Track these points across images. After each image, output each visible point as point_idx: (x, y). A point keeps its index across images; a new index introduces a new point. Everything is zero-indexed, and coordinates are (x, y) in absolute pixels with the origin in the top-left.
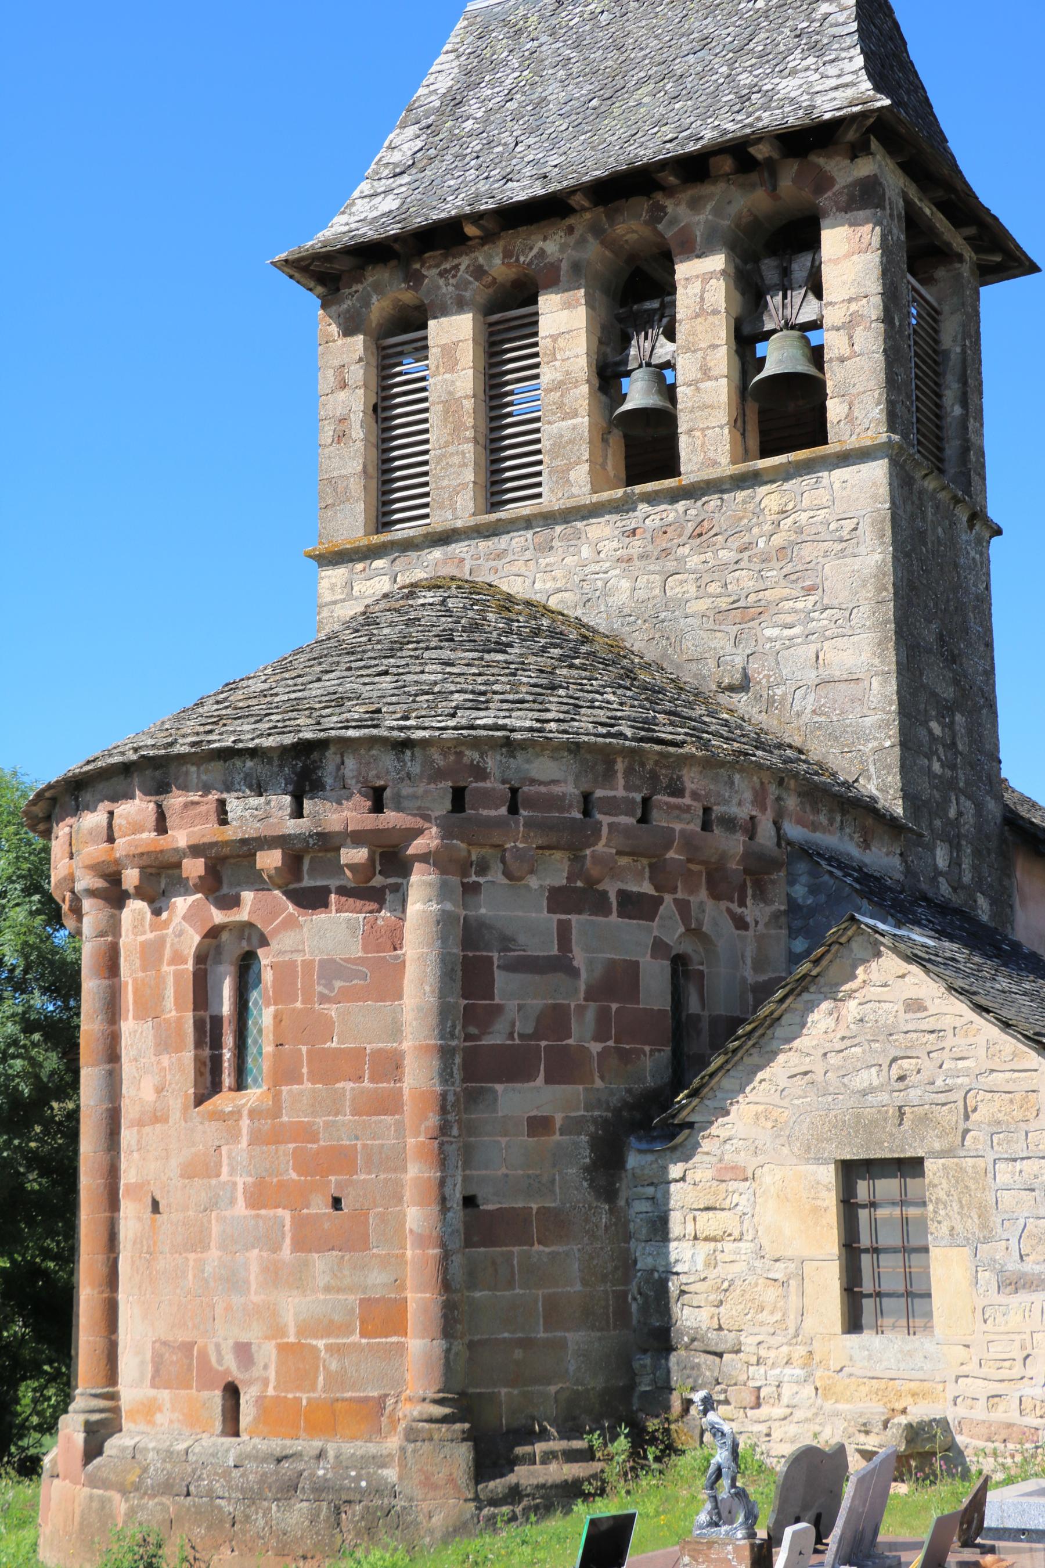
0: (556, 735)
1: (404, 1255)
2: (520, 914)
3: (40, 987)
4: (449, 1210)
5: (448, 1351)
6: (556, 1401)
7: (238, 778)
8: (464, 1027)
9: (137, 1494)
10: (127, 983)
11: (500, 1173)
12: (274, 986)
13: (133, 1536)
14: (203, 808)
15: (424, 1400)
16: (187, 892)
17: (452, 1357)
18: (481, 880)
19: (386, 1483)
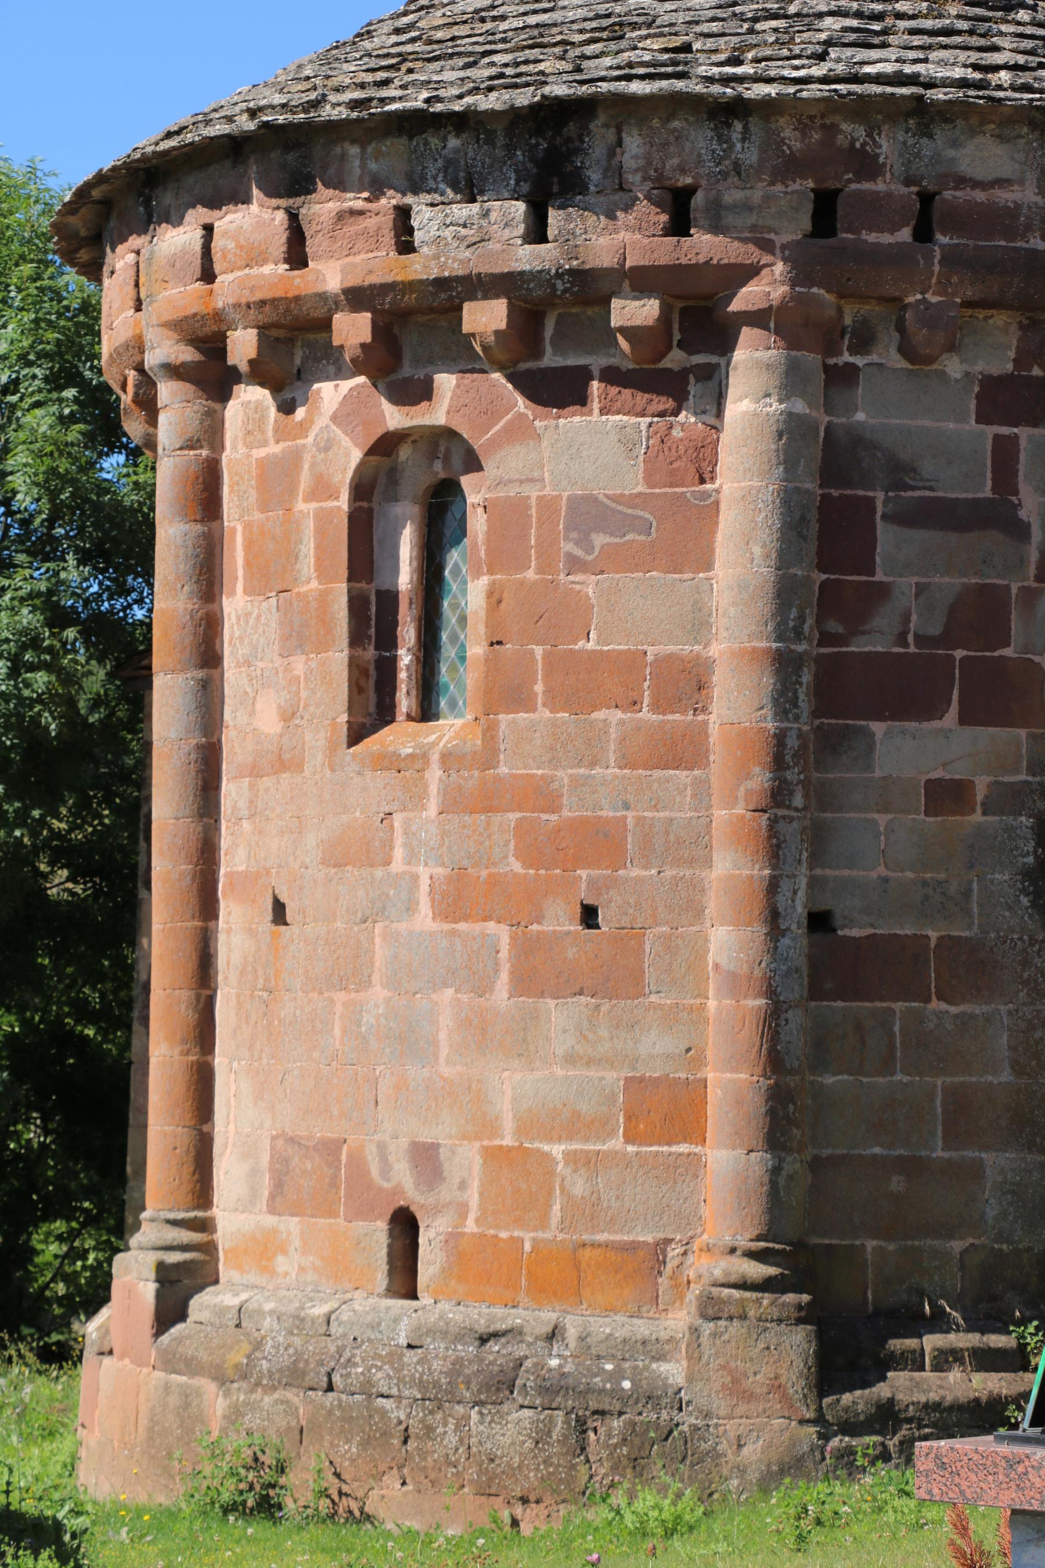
0: (1009, 94)
1: (703, 1007)
2: (927, 423)
3: (78, 550)
4: (783, 933)
5: (775, 1172)
6: (963, 1267)
7: (433, 168)
8: (819, 621)
9: (244, 1384)
10: (234, 530)
11: (874, 875)
12: (488, 541)
13: (237, 1452)
14: (370, 223)
15: (733, 1251)
16: (340, 374)
17: (782, 1181)
18: (859, 361)
19: (666, 1386)
